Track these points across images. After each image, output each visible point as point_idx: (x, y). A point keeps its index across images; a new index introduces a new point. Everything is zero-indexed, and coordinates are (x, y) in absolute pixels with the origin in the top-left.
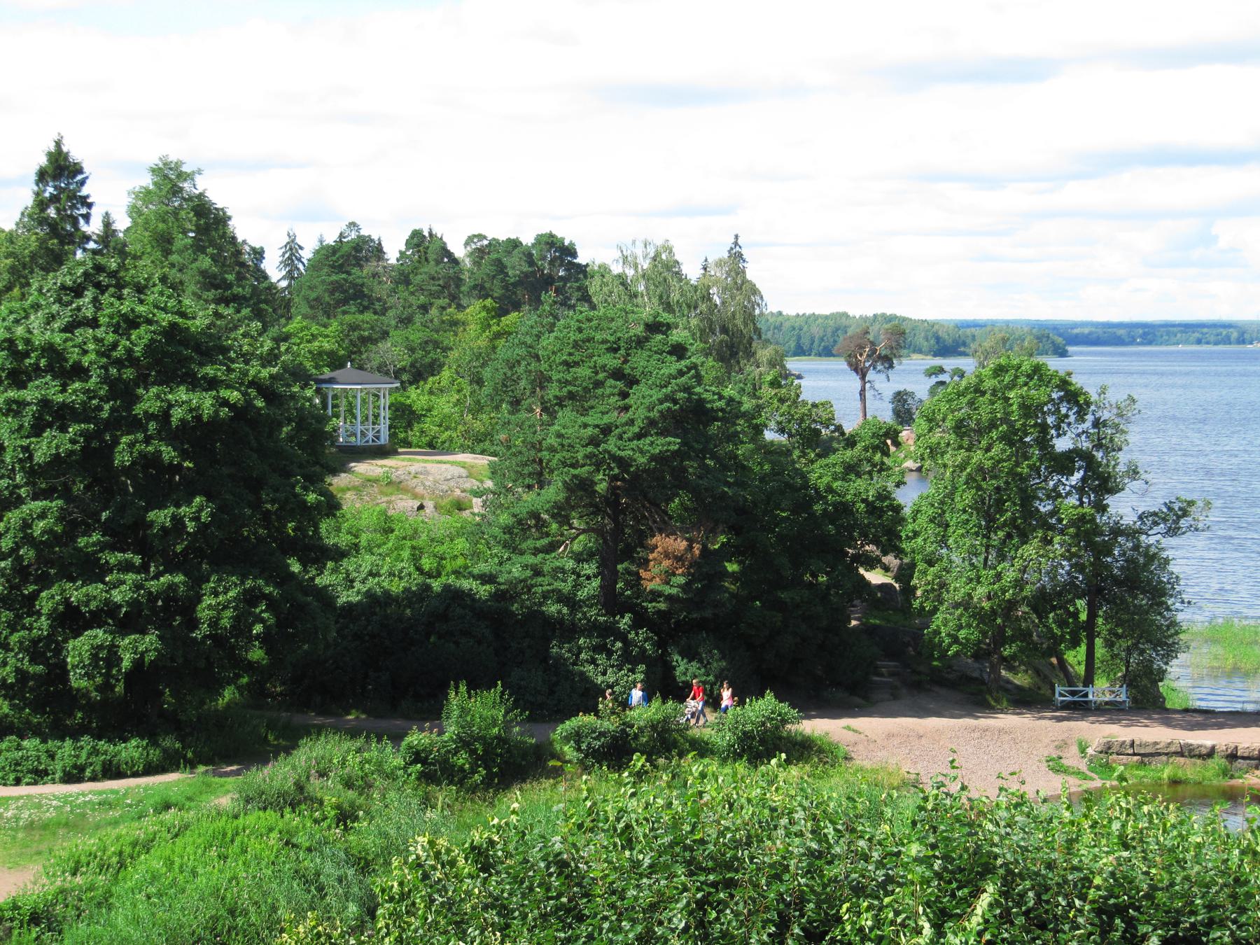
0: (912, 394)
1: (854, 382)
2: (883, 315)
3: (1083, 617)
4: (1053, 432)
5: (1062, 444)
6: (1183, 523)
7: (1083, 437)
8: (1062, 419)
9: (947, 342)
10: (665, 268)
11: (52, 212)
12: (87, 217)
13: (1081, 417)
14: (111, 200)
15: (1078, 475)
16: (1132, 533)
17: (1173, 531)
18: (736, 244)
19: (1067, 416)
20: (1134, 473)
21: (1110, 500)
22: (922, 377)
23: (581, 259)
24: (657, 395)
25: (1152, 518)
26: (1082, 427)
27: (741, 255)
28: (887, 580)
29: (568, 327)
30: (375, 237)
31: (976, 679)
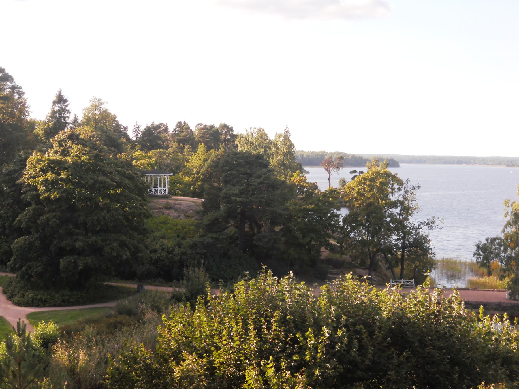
1: (327, 174)
2: (337, 152)
9: (358, 161)
10: (262, 135)
11: (57, 115)
12: (68, 117)
14: (77, 111)
17: (430, 228)
21: (410, 217)
23: (235, 132)
27: (288, 131)
30: (165, 124)
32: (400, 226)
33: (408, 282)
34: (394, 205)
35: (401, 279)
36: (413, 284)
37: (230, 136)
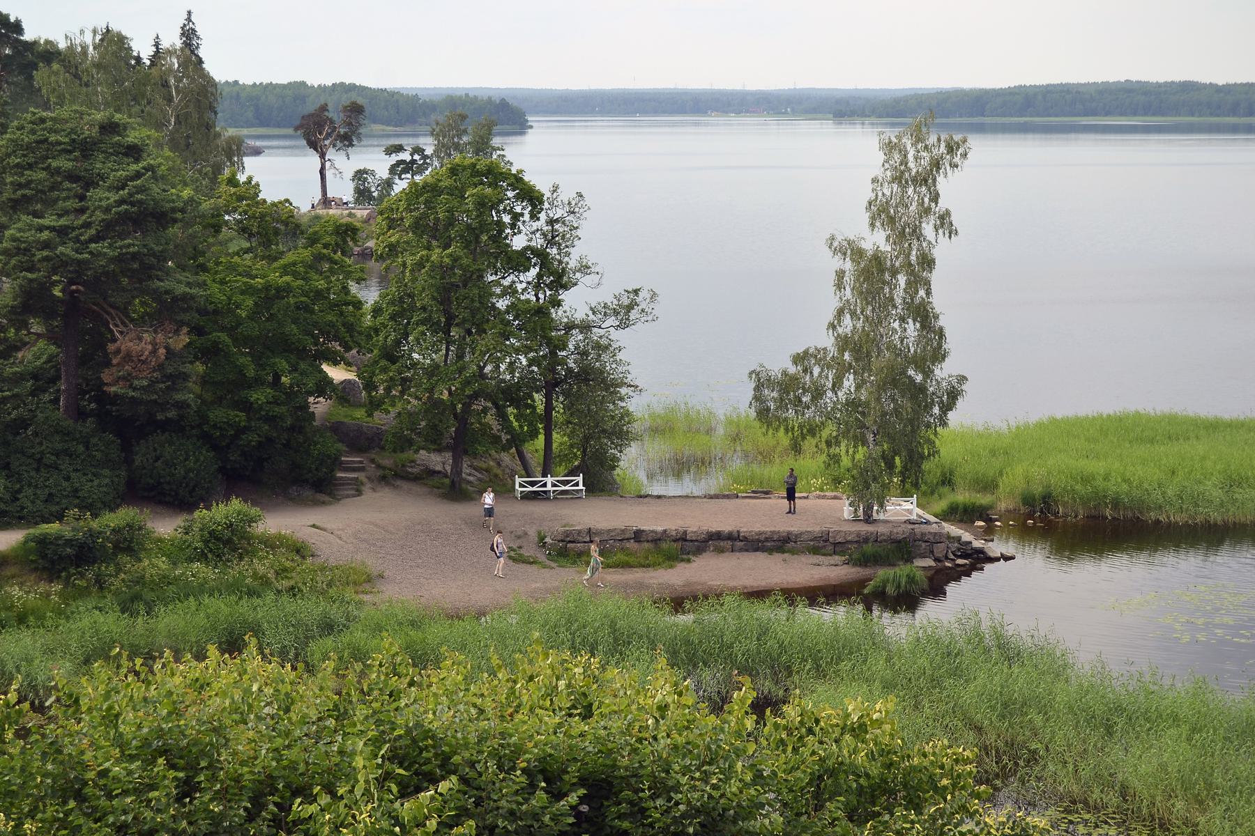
0: (373, 173)
1: (314, 160)
2: (342, 84)
3: (540, 408)
4: (508, 231)
5: (518, 243)
6: (634, 314)
7: (538, 235)
8: (516, 217)
9: (401, 110)
13: (534, 217)
15: (534, 272)
16: (586, 327)
17: (624, 325)
18: (189, 19)
19: (522, 215)
20: (585, 269)
21: (565, 296)
22: (383, 156)
23: (28, 36)
24: (114, 197)
25: (606, 311)
26: (536, 225)
28: (351, 376)
29: (20, 128)
31: (439, 472)
32: (537, 320)
33: (565, 483)
34: (518, 261)
35: (544, 475)
36: (581, 487)
37: (13, 48)
